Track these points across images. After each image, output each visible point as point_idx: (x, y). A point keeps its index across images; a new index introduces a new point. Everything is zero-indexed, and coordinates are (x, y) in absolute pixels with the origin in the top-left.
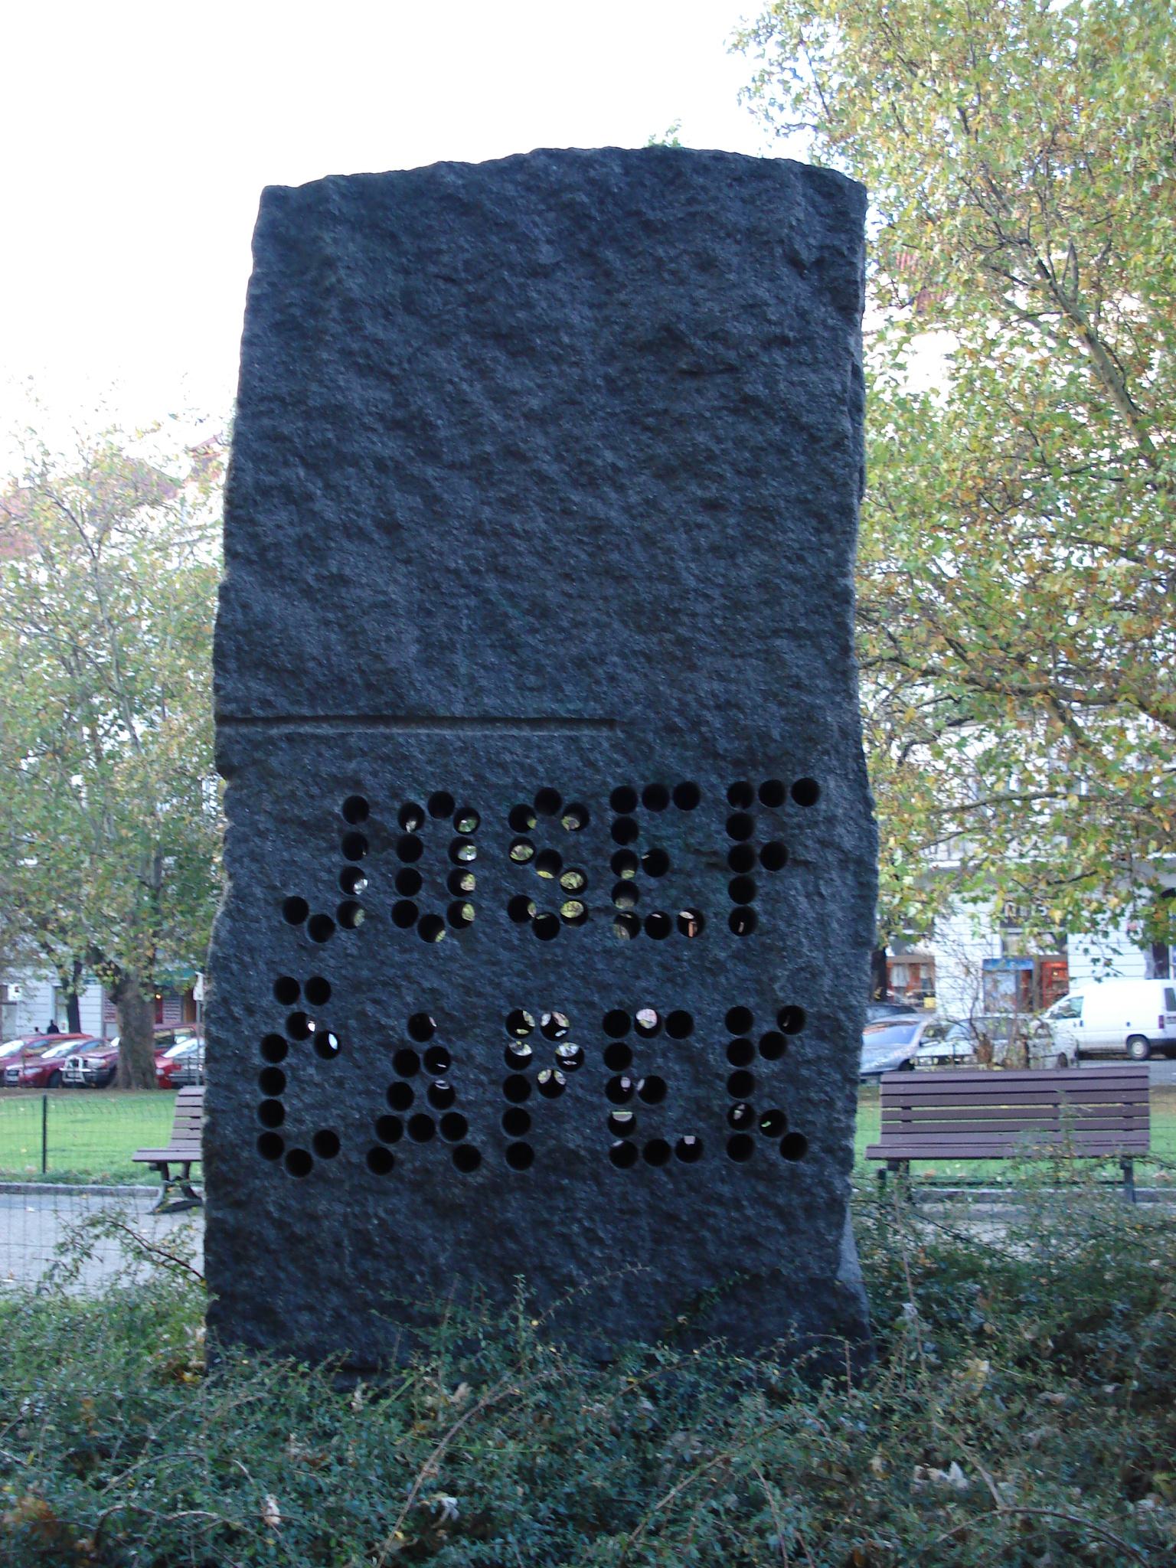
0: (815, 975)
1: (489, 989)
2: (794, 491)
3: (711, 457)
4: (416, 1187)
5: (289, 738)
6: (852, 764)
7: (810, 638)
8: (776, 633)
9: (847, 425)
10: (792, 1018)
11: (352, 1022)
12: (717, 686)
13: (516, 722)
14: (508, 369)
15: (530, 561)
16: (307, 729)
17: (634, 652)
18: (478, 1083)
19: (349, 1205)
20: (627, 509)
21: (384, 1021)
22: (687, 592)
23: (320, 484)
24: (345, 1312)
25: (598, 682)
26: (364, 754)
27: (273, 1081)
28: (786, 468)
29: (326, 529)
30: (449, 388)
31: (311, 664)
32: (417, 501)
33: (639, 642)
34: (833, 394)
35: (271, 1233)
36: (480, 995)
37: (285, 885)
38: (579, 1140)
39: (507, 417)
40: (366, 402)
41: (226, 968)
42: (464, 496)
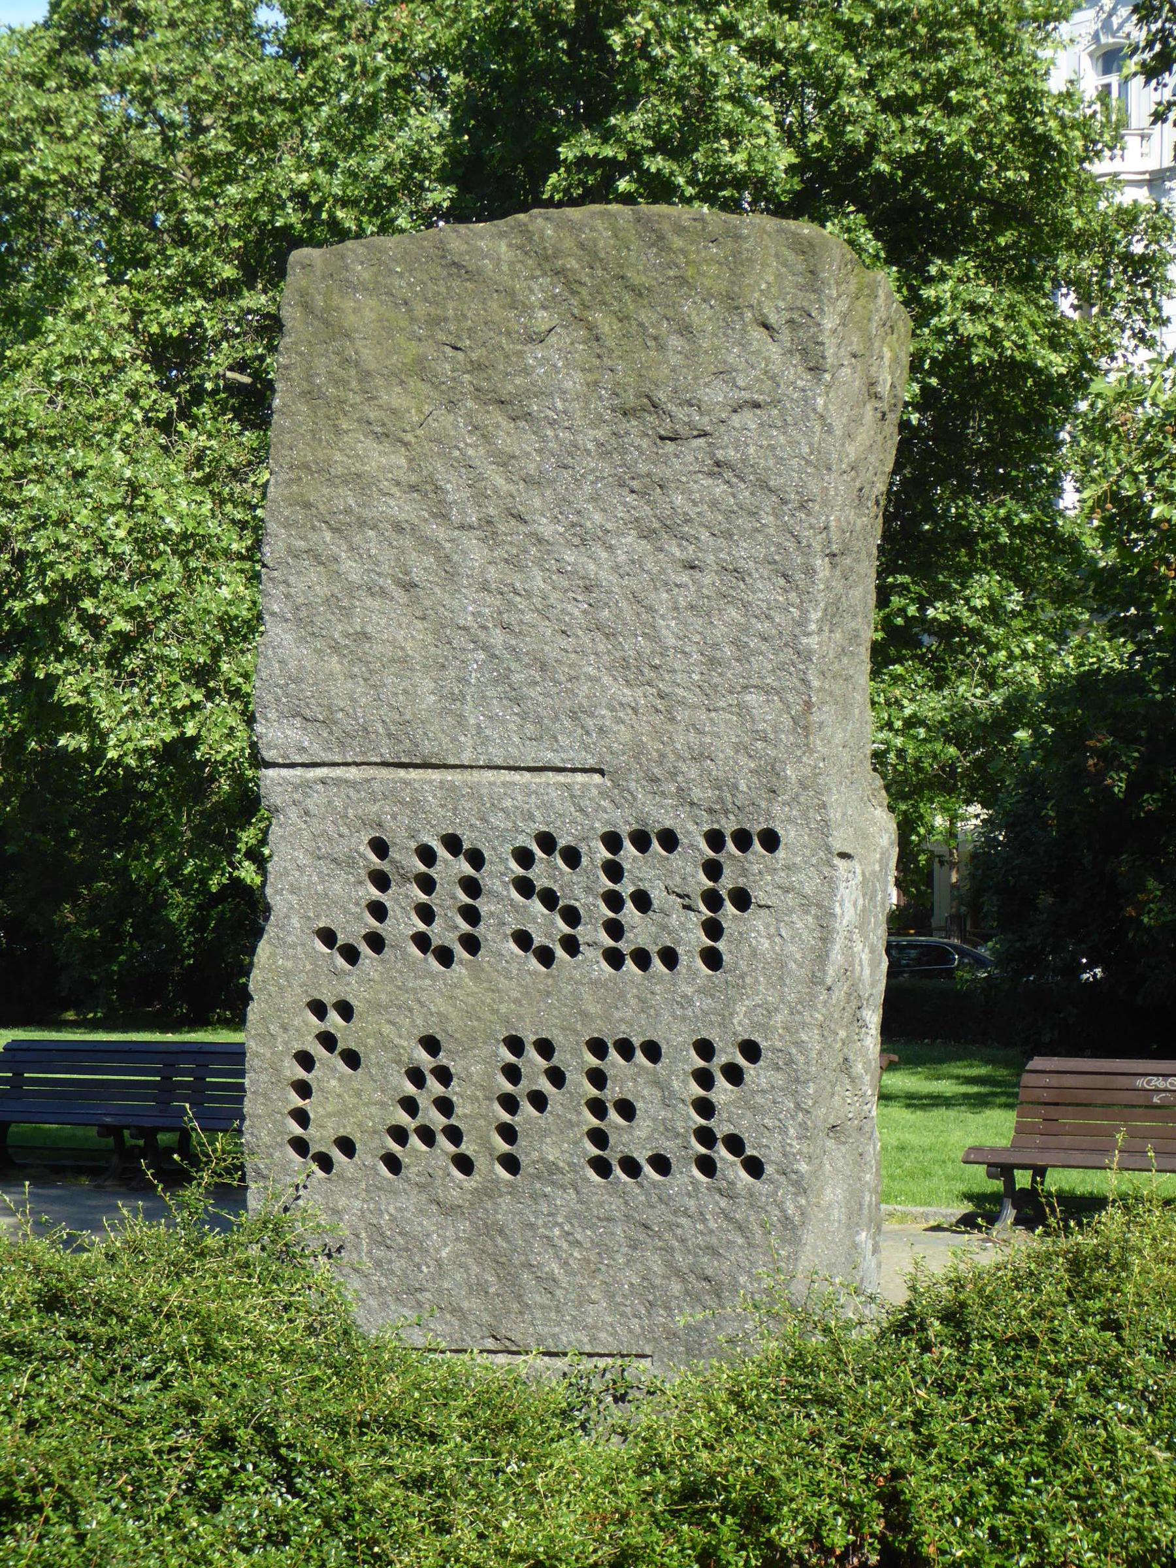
1: (488, 1016)
4: (422, 1187)
7: (778, 693)
11: (371, 1041)
15: (528, 617)
16: (338, 772)
17: (621, 704)
19: (364, 1201)
20: (616, 568)
21: (397, 1041)
22: (667, 649)
23: (345, 548)
26: (385, 797)
28: (757, 530)
29: (351, 589)
30: (456, 453)
31: (340, 715)
36: (479, 1019)
37: (318, 916)
39: (509, 480)
42: (474, 553)
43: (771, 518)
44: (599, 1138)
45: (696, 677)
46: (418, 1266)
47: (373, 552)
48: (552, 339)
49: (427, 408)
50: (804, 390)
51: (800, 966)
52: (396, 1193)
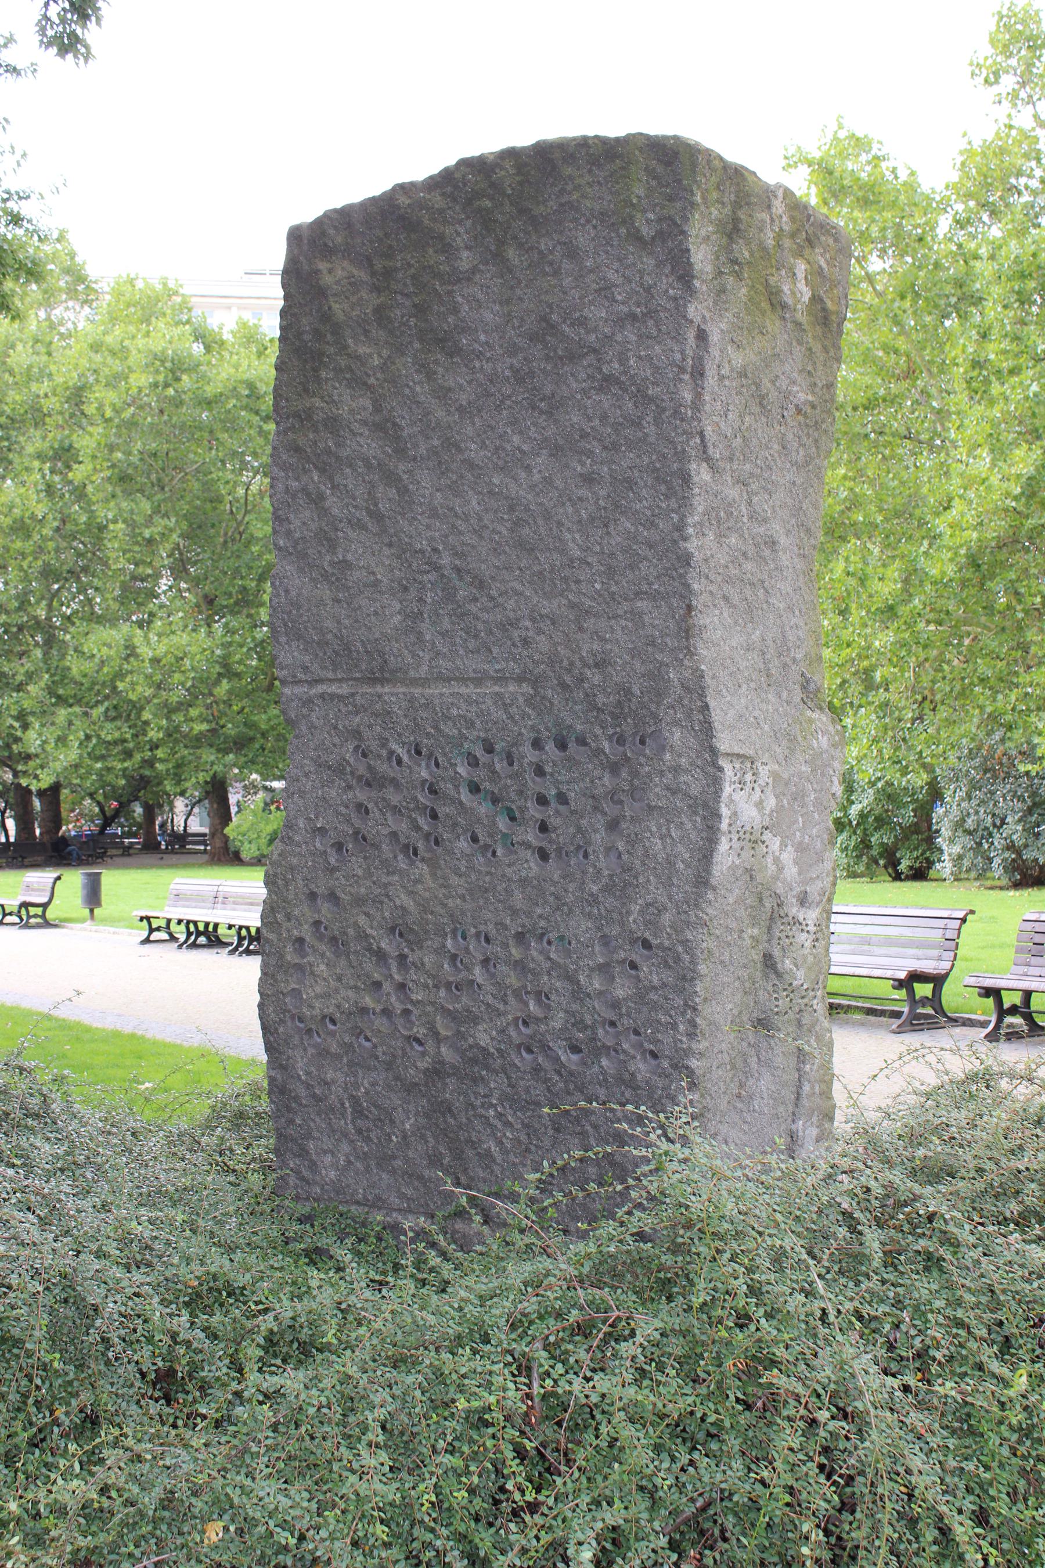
0: (661, 910)
2: (646, 460)
3: (584, 436)
4: (389, 1066)
5: (322, 696)
6: (697, 716)
9: (688, 396)
12: (596, 646)
13: (463, 680)
14: (447, 370)
15: (468, 538)
16: (333, 689)
17: (542, 616)
18: (426, 986)
21: (369, 931)
24: (352, 1159)
25: (514, 645)
30: (407, 391)
32: (393, 493)
34: (673, 364)
35: (302, 1092)
38: (487, 1038)
40: (352, 411)
41: (274, 883)
43: (653, 428)
45: (598, 586)
46: (389, 1135)
50: (676, 299)
51: (688, 866)
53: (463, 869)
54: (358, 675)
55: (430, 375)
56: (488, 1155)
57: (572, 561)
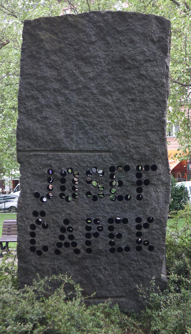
4: (66, 258)
5: (35, 155)
6: (165, 161)
7: (156, 131)
8: (147, 130)
10: (150, 220)
13: (87, 151)
15: (90, 113)
17: (114, 135)
19: (50, 262)
20: (113, 101)
23: (41, 95)
27: (33, 235)
29: (42, 106)
30: (71, 72)
31: (39, 138)
33: (116, 132)
34: (161, 73)
39: (85, 79)
40: (51, 75)
44: (111, 243)
47: (48, 96)
48: (96, 43)
49: (63, 60)
52: (59, 259)
53: (88, 202)
54: (49, 149)
55: (79, 68)
56: (100, 278)
57: (127, 121)
